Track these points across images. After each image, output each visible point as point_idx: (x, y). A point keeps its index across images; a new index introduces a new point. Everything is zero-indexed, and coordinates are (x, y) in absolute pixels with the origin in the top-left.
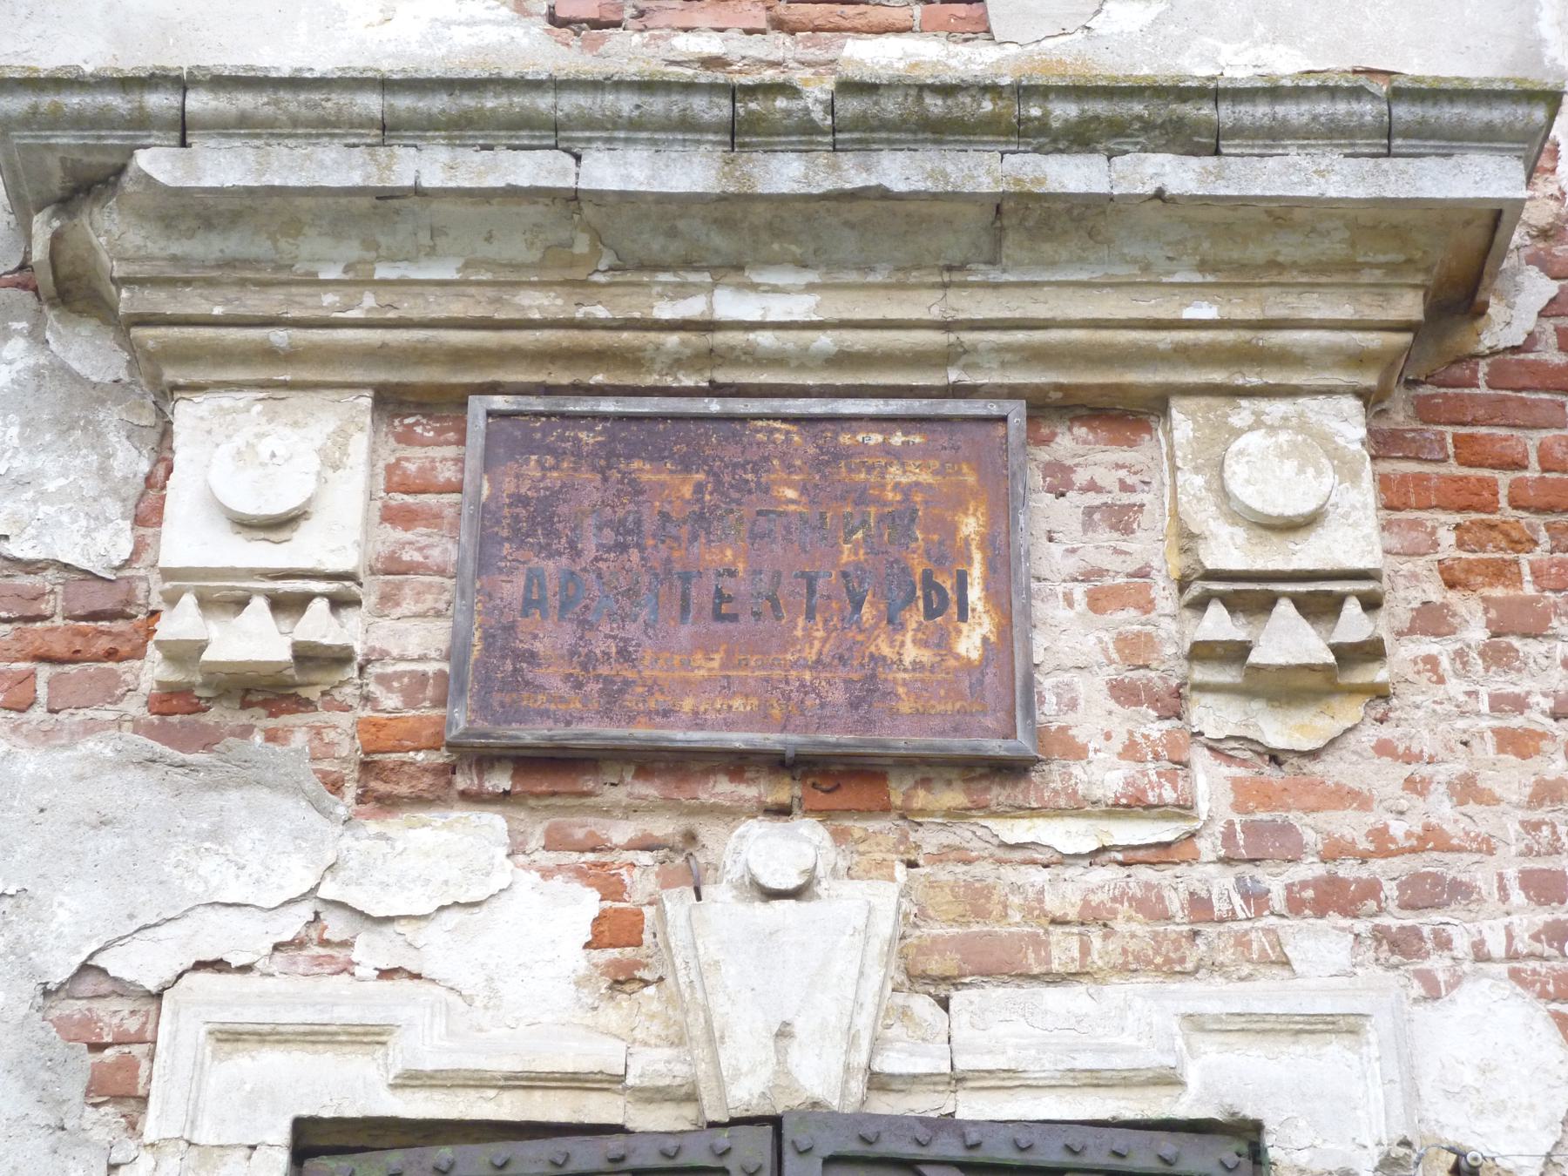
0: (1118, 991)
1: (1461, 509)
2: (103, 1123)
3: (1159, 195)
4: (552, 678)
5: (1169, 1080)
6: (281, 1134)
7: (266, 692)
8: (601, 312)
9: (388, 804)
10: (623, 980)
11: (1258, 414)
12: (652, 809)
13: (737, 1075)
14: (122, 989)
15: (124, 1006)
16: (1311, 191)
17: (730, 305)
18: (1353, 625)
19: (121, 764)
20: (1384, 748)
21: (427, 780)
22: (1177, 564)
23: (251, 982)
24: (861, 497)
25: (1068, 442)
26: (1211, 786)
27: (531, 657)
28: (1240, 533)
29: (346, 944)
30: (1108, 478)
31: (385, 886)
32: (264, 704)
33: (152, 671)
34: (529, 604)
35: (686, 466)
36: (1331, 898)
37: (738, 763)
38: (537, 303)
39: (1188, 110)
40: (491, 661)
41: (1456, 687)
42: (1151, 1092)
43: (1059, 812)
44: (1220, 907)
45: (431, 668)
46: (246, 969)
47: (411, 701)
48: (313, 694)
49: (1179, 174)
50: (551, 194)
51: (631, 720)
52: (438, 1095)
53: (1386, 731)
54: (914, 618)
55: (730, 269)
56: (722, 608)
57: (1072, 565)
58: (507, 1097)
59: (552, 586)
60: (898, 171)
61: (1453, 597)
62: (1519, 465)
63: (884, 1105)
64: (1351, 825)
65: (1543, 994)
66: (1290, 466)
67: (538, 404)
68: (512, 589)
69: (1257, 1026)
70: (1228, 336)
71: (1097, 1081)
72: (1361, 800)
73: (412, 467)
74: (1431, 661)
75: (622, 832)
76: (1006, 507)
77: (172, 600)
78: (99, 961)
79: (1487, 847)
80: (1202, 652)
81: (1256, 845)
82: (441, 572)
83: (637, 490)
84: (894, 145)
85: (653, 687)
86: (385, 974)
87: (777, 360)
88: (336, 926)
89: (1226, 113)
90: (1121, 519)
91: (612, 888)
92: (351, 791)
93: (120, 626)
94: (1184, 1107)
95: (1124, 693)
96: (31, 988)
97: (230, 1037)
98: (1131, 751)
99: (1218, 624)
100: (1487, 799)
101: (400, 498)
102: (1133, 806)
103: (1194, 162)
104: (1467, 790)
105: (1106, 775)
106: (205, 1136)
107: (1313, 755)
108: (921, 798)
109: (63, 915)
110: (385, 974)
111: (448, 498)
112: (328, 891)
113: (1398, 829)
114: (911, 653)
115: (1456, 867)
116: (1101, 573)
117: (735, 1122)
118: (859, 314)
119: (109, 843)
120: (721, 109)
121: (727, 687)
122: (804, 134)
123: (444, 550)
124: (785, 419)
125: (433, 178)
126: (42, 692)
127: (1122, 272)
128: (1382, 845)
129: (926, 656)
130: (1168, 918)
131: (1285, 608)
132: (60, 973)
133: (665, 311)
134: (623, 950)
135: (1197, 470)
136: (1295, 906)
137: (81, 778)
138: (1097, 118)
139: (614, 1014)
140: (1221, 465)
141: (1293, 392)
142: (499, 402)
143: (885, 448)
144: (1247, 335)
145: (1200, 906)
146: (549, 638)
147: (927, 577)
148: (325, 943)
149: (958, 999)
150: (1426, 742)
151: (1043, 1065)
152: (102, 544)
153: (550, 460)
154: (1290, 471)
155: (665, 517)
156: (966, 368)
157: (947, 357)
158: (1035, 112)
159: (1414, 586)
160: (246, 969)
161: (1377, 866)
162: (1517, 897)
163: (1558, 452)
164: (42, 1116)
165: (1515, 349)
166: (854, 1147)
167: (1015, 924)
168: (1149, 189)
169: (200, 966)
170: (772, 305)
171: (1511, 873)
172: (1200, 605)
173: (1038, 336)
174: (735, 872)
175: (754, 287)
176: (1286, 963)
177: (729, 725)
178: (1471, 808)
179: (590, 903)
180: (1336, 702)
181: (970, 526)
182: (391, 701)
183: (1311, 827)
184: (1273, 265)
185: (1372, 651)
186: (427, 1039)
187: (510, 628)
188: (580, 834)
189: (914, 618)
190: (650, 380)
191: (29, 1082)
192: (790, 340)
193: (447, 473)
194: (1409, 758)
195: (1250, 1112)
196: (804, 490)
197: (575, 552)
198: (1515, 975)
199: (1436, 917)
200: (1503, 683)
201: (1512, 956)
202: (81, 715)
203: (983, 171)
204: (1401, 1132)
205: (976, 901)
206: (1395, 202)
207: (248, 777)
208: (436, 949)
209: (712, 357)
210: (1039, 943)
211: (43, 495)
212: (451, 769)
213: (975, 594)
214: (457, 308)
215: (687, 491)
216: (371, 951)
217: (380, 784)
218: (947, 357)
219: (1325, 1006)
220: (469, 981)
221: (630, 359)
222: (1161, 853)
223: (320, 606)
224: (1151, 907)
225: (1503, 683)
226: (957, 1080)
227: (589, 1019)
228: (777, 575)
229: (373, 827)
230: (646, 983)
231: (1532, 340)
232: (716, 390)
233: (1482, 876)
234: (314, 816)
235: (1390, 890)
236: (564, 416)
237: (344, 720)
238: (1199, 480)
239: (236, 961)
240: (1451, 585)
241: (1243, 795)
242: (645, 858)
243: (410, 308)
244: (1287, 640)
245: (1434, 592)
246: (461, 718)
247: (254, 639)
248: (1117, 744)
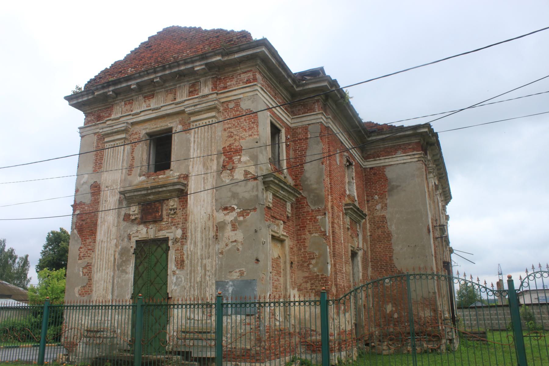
18: (175, 211)
36: (174, 225)
40: (142, 218)
49: (165, 189)
76: (162, 206)
81: (172, 222)
102: (166, 221)
122: (149, 189)
170: (151, 197)
186: (140, 237)
244: (172, 212)
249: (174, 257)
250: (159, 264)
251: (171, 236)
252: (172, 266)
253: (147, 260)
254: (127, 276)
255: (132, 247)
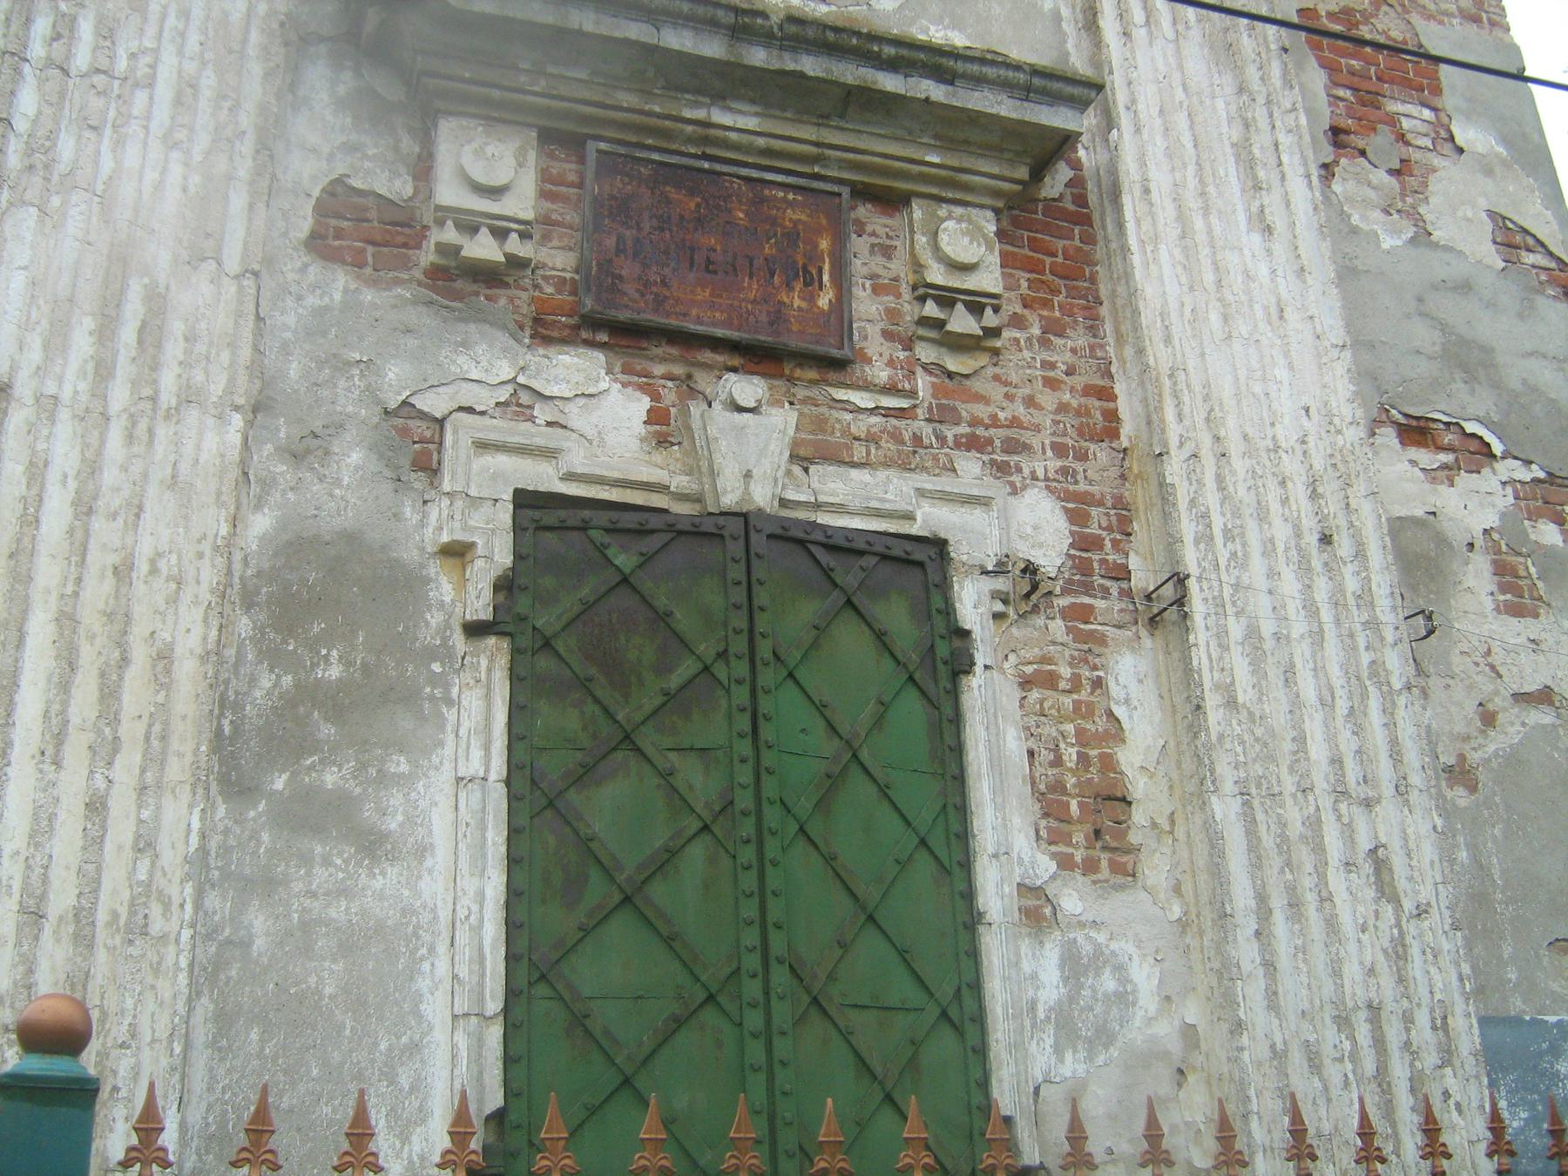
0: (882, 474)
1: (1030, 272)
2: (418, 480)
3: (927, 99)
4: (630, 289)
5: (909, 517)
6: (508, 496)
7: (488, 276)
8: (657, 109)
9: (547, 341)
10: (663, 441)
11: (950, 212)
12: (673, 360)
13: (725, 492)
14: (423, 415)
15: (424, 425)
16: (993, 111)
17: (720, 117)
18: (990, 319)
19: (415, 302)
20: (996, 378)
21: (566, 332)
22: (911, 278)
23: (486, 421)
24: (774, 222)
25: (863, 211)
26: (923, 384)
27: (620, 278)
28: (942, 267)
29: (531, 407)
30: (881, 231)
31: (548, 381)
32: (484, 282)
33: (427, 256)
34: (619, 251)
35: (692, 193)
36: (972, 444)
37: (716, 344)
38: (627, 99)
39: (944, 61)
40: (598, 276)
41: (1027, 354)
42: (902, 522)
43: (858, 388)
44: (926, 441)
45: (568, 275)
46: (483, 413)
47: (559, 292)
48: (510, 280)
50: (644, 45)
51: (668, 315)
52: (582, 485)
53: (997, 370)
54: (798, 285)
55: (719, 98)
56: (709, 266)
57: (864, 271)
58: (614, 490)
59: (630, 243)
60: (811, 65)
61: (1026, 312)
62: (1054, 255)
63: (785, 513)
64: (981, 411)
65: (1059, 498)
66: (966, 240)
67: (622, 150)
68: (611, 242)
69: (945, 497)
70: (943, 173)
71: (878, 514)
72: (986, 400)
73: (554, 171)
74: (1017, 340)
75: (659, 370)
76: (840, 242)
77: (441, 223)
78: (412, 400)
79: (1037, 429)
80: (924, 321)
81: (942, 415)
82: (571, 228)
83: (669, 202)
84: (808, 52)
85: (677, 300)
86: (549, 424)
87: (736, 147)
88: (525, 398)
89: (960, 66)
90: (887, 252)
91: (656, 397)
92: (528, 332)
93: (407, 231)
94: (915, 530)
95: (888, 335)
96: (378, 409)
97: (483, 446)
98: (891, 363)
99: (931, 309)
100: (1039, 407)
101: (549, 188)
102: (891, 389)
103: (943, 87)
104: (1030, 402)
105: (882, 375)
106: (473, 492)
107: (967, 376)
108: (798, 373)
109: (391, 375)
110: (549, 424)
111: (572, 190)
112: (521, 379)
113: (1002, 415)
114: (797, 303)
115: (1026, 437)
116: (878, 276)
117: (722, 514)
118: (779, 132)
119: (412, 342)
120: (730, 19)
121: (712, 306)
122: (767, 38)
123: (572, 217)
124: (739, 177)
125: (589, 27)
126: (370, 259)
127: (900, 133)
128: (995, 422)
129: (804, 305)
130: (903, 443)
131: (960, 306)
132: (393, 405)
133: (688, 113)
134: (663, 428)
135: (923, 234)
136: (958, 445)
137: (395, 306)
138: (903, 57)
139: (658, 457)
140: (936, 233)
141: (965, 204)
142: (603, 146)
143: (784, 200)
144: (951, 173)
145: (917, 439)
146: (628, 269)
147: (805, 267)
148: (519, 405)
149: (812, 469)
150: (1014, 378)
151: (857, 504)
152: (400, 187)
153: (627, 180)
154: (965, 242)
155: (682, 217)
156: (823, 166)
157: (817, 159)
158: (876, 48)
159: (1012, 307)
160: (483, 413)
161: (992, 431)
162: (1049, 453)
163: (1071, 252)
164: (388, 473)
165: (1054, 200)
166: (779, 531)
167: (837, 437)
168: (923, 96)
169: (461, 409)
171: (1047, 442)
172: (922, 299)
173: (859, 157)
174: (723, 397)
175: (730, 109)
176: (954, 470)
177: (714, 325)
178: (1031, 410)
179: (646, 402)
180: (977, 354)
181: (824, 244)
182: (550, 290)
183: (965, 410)
184: (967, 142)
185: (994, 332)
186: (577, 459)
187: (610, 261)
188: (638, 368)
189: (798, 285)
190: (674, 147)
191: (381, 456)
192: (745, 138)
193: (572, 177)
194: (1007, 384)
195: (942, 535)
196: (747, 214)
197: (640, 229)
198: (1047, 487)
199: (1016, 458)
200: (1046, 356)
201: (1047, 479)
202: (391, 274)
203: (850, 73)
204: (1005, 551)
205: (820, 424)
206: (1029, 123)
207: (480, 317)
208: (575, 415)
209: (706, 141)
210: (849, 448)
211: (366, 157)
212: (577, 328)
213: (826, 278)
214: (586, 94)
215: (692, 206)
216: (542, 413)
217: (544, 330)
218: (817, 159)
219: (975, 492)
220: (590, 432)
221: (666, 134)
222: (900, 413)
223: (514, 236)
224: (896, 437)
225: (1046, 356)
226: (817, 506)
227: (647, 458)
228: (735, 256)
229: (541, 351)
230: (673, 444)
231: (1061, 198)
232: (705, 157)
233: (1035, 442)
234: (512, 342)
235: (997, 443)
236: (634, 158)
237: (524, 295)
238: (924, 239)
239: (479, 408)
240: (1025, 306)
241: (937, 391)
242: (670, 384)
243: (564, 90)
244: (962, 322)
245: (1019, 309)
246: (589, 303)
247: (483, 248)
248: (886, 358)
249: (1014, 744)
250: (858, 789)
251: (975, 535)
252: (1006, 839)
253: (714, 726)
254: (388, 879)
255: (457, 552)
